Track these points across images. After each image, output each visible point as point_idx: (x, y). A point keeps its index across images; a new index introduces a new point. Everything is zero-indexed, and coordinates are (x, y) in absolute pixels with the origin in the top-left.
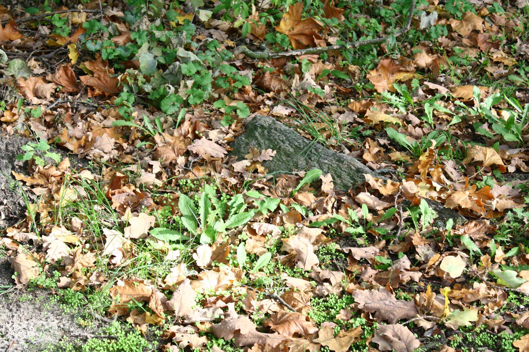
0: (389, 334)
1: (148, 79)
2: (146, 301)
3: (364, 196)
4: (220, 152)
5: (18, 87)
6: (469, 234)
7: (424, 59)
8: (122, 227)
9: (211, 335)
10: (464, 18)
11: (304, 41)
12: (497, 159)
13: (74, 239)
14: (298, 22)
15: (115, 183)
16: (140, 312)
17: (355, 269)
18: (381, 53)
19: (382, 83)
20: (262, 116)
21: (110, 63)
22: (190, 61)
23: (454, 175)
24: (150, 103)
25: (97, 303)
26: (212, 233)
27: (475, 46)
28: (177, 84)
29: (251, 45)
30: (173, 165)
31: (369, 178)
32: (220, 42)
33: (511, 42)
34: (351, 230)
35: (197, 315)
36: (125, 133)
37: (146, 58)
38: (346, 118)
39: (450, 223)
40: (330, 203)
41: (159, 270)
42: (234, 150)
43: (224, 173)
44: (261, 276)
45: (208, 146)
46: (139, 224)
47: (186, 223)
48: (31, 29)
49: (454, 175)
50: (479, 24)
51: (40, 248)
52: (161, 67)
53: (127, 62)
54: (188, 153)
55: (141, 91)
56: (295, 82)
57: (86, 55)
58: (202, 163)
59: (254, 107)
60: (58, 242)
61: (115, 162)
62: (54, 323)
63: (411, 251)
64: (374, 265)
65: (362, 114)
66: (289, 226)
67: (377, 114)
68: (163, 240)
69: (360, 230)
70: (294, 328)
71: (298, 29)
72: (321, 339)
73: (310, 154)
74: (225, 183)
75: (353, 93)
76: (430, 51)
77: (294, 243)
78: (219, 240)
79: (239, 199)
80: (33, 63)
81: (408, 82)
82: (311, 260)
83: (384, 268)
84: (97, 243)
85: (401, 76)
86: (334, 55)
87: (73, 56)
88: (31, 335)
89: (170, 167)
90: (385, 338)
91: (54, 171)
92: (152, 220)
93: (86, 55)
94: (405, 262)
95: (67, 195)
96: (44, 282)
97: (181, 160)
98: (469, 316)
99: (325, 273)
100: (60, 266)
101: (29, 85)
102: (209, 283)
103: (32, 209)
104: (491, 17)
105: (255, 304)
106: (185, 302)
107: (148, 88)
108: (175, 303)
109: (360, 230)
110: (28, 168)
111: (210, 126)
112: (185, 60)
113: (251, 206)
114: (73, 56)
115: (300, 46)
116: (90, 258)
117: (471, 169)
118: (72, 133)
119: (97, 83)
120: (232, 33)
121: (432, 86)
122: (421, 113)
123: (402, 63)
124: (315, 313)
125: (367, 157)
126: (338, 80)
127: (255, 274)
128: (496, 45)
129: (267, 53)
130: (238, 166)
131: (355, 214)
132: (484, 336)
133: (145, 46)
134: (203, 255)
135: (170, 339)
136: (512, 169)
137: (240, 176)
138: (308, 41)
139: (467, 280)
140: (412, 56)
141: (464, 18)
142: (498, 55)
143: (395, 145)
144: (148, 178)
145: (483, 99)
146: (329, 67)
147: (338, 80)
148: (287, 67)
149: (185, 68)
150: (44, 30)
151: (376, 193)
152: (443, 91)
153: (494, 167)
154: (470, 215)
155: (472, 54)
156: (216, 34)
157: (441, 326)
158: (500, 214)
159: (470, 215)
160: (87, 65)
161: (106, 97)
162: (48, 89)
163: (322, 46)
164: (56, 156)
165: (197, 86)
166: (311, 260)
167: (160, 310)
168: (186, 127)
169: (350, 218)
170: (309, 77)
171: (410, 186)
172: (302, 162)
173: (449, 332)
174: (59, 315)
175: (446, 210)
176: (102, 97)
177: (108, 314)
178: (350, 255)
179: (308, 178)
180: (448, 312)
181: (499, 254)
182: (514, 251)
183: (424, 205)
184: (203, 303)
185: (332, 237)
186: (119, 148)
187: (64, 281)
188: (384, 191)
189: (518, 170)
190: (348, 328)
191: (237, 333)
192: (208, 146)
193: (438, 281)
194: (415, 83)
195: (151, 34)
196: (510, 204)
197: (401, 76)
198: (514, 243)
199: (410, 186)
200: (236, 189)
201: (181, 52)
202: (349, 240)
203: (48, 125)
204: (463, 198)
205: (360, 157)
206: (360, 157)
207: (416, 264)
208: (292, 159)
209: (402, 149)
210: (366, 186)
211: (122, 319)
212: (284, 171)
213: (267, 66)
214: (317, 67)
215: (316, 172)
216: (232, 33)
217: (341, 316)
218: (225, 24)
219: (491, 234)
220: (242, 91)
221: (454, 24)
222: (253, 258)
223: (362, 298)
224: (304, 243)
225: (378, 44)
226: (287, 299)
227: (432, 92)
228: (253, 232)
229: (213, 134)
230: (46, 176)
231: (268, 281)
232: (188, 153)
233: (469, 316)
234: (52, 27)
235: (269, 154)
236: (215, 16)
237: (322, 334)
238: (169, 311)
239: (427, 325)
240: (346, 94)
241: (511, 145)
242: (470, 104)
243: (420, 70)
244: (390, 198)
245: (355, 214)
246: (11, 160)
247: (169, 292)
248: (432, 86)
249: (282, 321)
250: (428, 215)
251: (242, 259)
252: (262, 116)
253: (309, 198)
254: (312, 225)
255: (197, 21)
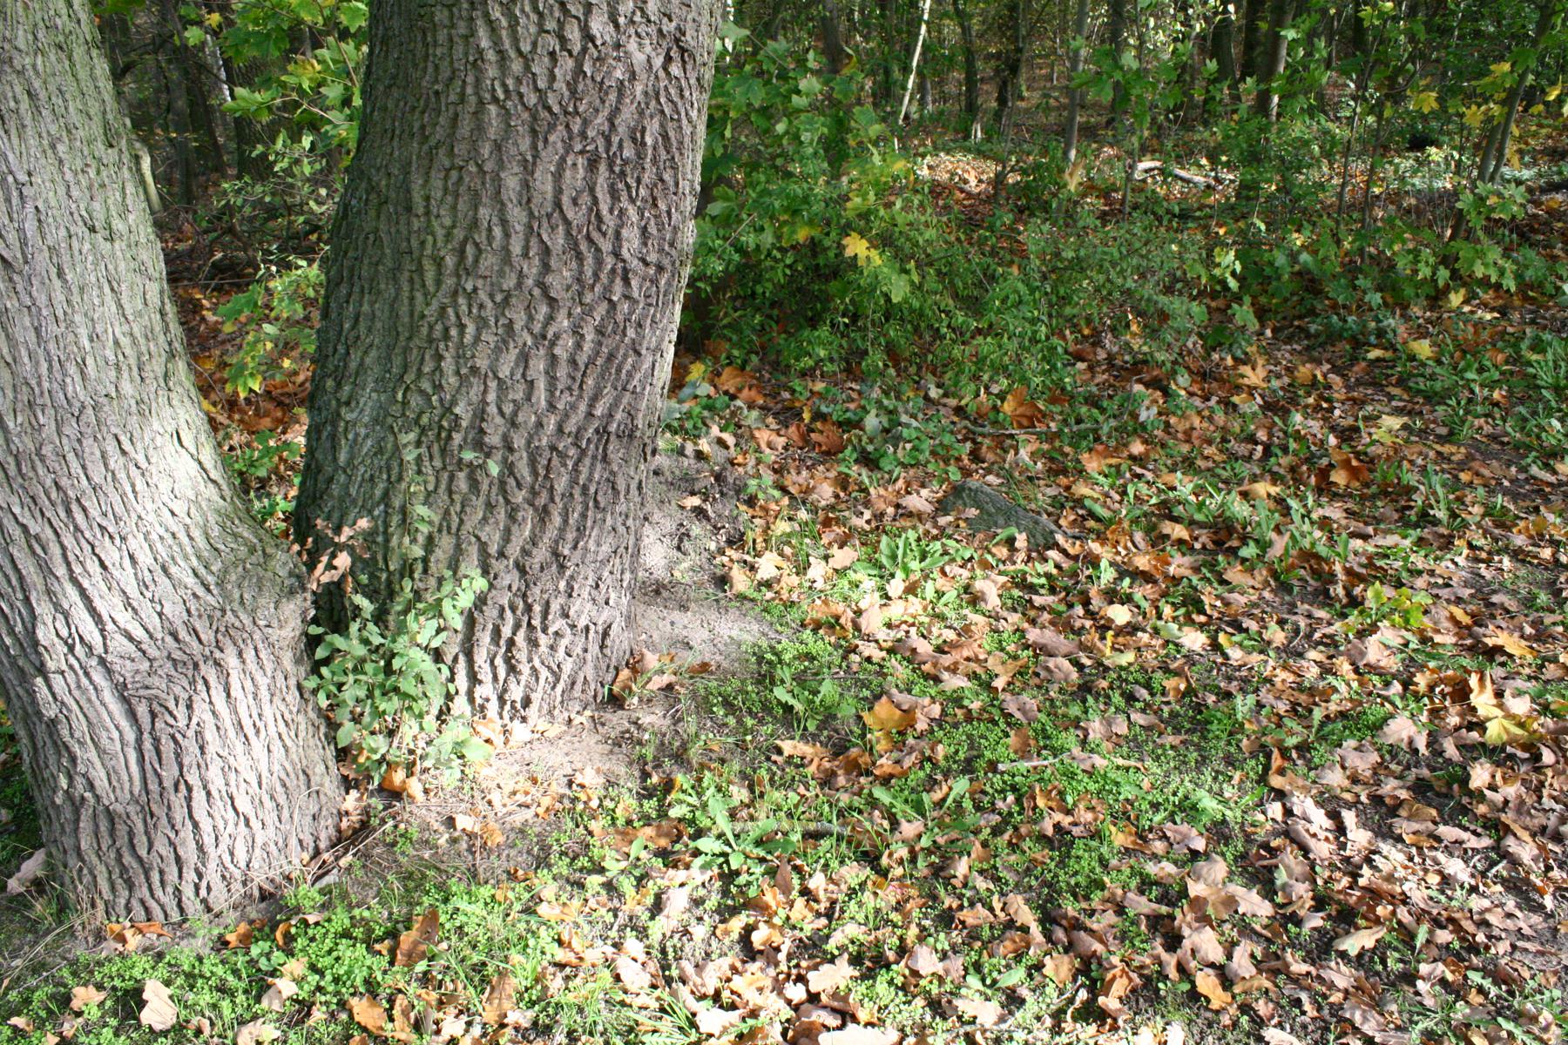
0: (1051, 665)
1: (871, 441)
2: (837, 618)
3: (1053, 554)
4: (929, 508)
5: (753, 437)
6: (1141, 593)
7: (1137, 448)
8: (826, 558)
9: (891, 651)
10: (1184, 416)
11: (1025, 422)
12: (1185, 535)
13: (784, 565)
14: (1021, 404)
15: (827, 523)
16: (831, 627)
17: (1032, 613)
18: (1097, 439)
19: (1093, 465)
20: (974, 482)
21: (840, 424)
22: (911, 426)
23: (1142, 545)
24: (869, 461)
25: (794, 616)
26: (907, 571)
27: (1188, 441)
28: (896, 447)
29: (975, 422)
30: (882, 514)
31: (1060, 538)
32: (946, 418)
33: (1224, 440)
34: (1036, 581)
35: (883, 635)
36: (843, 482)
37: (872, 422)
38: (1051, 492)
39: (1127, 581)
40: (1021, 556)
41: (854, 596)
42: (942, 507)
43: (928, 526)
44: (946, 610)
45: (919, 501)
46: (842, 557)
47: (884, 561)
48: (774, 395)
49: (1142, 545)
50: (1196, 421)
51: (753, 568)
52: (886, 431)
53: (858, 424)
54: (898, 506)
55: (864, 450)
56: (1010, 456)
57: (818, 416)
58: (910, 515)
59: (967, 474)
60: (768, 565)
61: (832, 508)
62: (755, 627)
63: (1086, 603)
64: (1051, 611)
65: (1068, 488)
66: (978, 572)
67: (1081, 489)
68: (864, 576)
69: (1043, 581)
70: (966, 653)
71: (1020, 411)
72: (989, 664)
73: (1009, 515)
74: (927, 533)
75: (1065, 472)
76: (1145, 442)
77: (979, 585)
78: (913, 578)
79: (937, 545)
80: (770, 420)
81: (1118, 467)
82: (993, 601)
83: (1059, 614)
84: (802, 568)
85: (1114, 461)
86: (1051, 437)
87: (806, 416)
88: (734, 633)
89: (879, 516)
90: (1047, 669)
91: (773, 506)
92: (855, 555)
93: (818, 416)
94: (1079, 610)
95: (782, 527)
96: (752, 594)
97: (890, 510)
98: (1128, 658)
99: (1005, 614)
100: (768, 584)
101: (763, 436)
102: (896, 611)
103: (750, 536)
104: (1211, 419)
105: (935, 631)
106: (873, 622)
107: (870, 448)
108: (863, 622)
109: (1043, 581)
110: (751, 502)
111: (923, 486)
112: (908, 426)
113: (945, 553)
114: (806, 416)
115: (1021, 426)
116: (795, 580)
117: (1158, 540)
118: (796, 479)
119: (824, 440)
120: (959, 410)
121: (1139, 471)
122: (1124, 493)
123: (1116, 449)
124: (988, 643)
125: (1062, 522)
126: (1052, 459)
127: (940, 608)
128: (1210, 442)
129: (988, 429)
130: (942, 521)
131: (1041, 568)
132: (1139, 676)
133: (873, 412)
134: (896, 587)
135: (854, 650)
136: (1197, 546)
137: (942, 529)
138: (1029, 421)
139: (1132, 629)
140: (1126, 445)
141: (1184, 416)
142: (1208, 451)
143: (1092, 515)
144: (859, 522)
145: (1185, 486)
146: (1046, 446)
147: (1052, 459)
148: (1003, 443)
149: (906, 433)
150: (786, 395)
151: (1064, 552)
152: (1150, 476)
153: (1180, 541)
154: (1147, 577)
155: (1185, 448)
156: (943, 411)
157: (1100, 664)
158: (1176, 580)
159: (1147, 577)
160: (819, 425)
161: (830, 454)
162: (781, 442)
163: (1040, 428)
164: (777, 494)
165: (915, 448)
166: (993, 601)
167: (849, 626)
168: (900, 484)
169: (1037, 572)
170: (1024, 454)
171: (1095, 547)
172: (1001, 521)
173: (1107, 669)
174: (760, 621)
175: (1123, 571)
176: (828, 453)
177: (803, 625)
178: (1030, 601)
179: (1003, 534)
180: (1108, 652)
181: (1167, 611)
182: (1182, 611)
183: (1104, 564)
184: (889, 626)
185: (1017, 585)
186: (837, 496)
187: (770, 595)
188: (1071, 551)
189: (1204, 547)
190: (1015, 658)
191: (914, 650)
192: (919, 501)
193: (1104, 627)
194: (1124, 467)
195: (879, 402)
196: (1188, 573)
197: (1114, 461)
198: (1184, 604)
199: (1095, 547)
200: (935, 538)
201: (904, 418)
202: (1032, 589)
203: (775, 471)
204: (1142, 562)
205: (1056, 523)
206: (1056, 523)
207: (1090, 614)
208: (994, 518)
209: (1098, 519)
210: (1056, 546)
211: (815, 631)
212: (984, 526)
213: (987, 441)
214: (1030, 448)
215: (1013, 530)
216: (959, 410)
217: (1011, 648)
218: (953, 402)
219: (1164, 594)
220: (958, 459)
221: (1173, 420)
222: (940, 594)
223: (1033, 635)
224: (990, 588)
225: (1095, 431)
226: (966, 631)
227: (1139, 477)
228: (944, 573)
229: (925, 492)
230: (765, 509)
231: (951, 614)
232: (898, 506)
233: (1128, 658)
234: (793, 392)
235: (973, 512)
236: (946, 395)
237: (991, 661)
238: (857, 627)
239: (1087, 662)
240: (1057, 470)
241: (1201, 525)
242: (1174, 489)
243: (1133, 458)
244: (1075, 558)
245: (1041, 568)
246: (738, 492)
247: (859, 613)
248: (1139, 471)
249: (954, 646)
250: (1107, 575)
251: (930, 593)
252: (974, 482)
253: (1003, 552)
254: (1000, 573)
255: (927, 398)
